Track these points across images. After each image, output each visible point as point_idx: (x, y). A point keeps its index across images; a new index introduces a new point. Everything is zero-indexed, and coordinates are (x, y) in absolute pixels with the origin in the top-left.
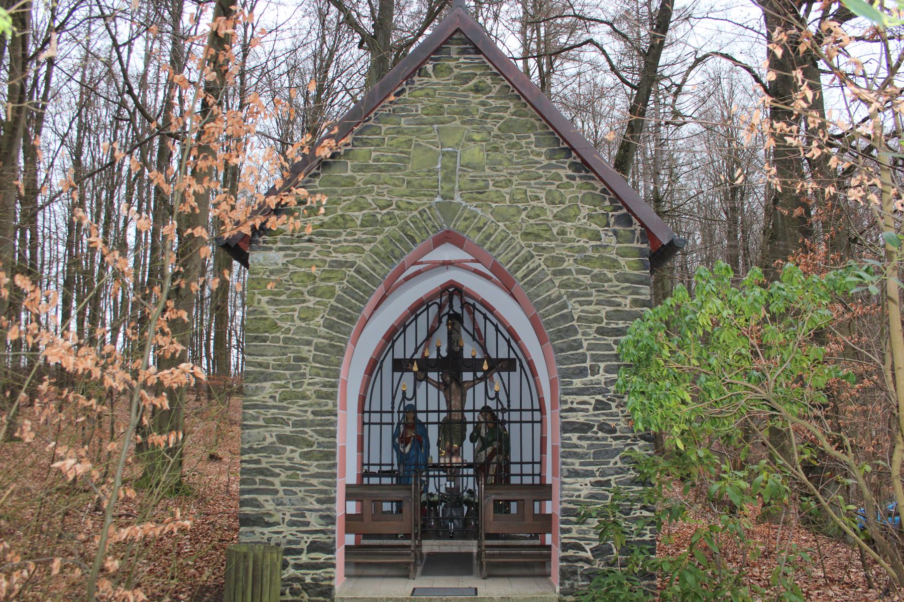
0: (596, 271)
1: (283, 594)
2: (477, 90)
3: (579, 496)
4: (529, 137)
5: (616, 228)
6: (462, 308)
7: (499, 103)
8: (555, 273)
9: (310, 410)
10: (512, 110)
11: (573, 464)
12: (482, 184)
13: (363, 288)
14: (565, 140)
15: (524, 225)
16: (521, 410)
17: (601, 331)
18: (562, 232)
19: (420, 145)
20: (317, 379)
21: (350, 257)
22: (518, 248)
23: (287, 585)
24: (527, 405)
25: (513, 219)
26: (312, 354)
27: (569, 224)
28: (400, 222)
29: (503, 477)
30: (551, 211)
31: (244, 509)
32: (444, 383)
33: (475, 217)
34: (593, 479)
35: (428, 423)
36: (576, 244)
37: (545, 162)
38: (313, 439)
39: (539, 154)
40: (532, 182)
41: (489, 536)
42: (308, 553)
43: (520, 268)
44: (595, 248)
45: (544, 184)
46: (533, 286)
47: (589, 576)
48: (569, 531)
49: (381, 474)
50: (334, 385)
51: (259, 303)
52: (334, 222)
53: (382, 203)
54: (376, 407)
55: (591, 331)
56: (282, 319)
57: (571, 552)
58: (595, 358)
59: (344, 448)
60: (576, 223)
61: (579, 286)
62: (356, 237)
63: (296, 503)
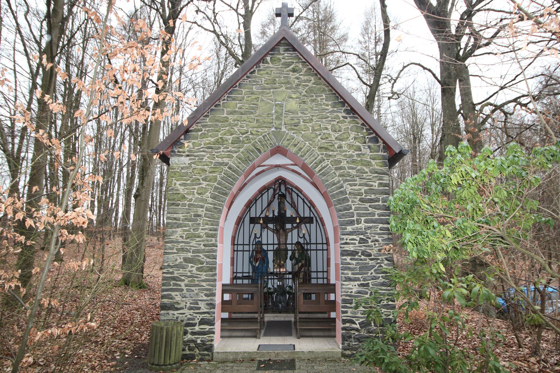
0: (359, 167)
1: (184, 350)
2: (294, 71)
3: (352, 292)
4: (322, 96)
5: (370, 144)
6: (286, 190)
7: (306, 78)
8: (336, 169)
9: (202, 243)
10: (313, 81)
11: (348, 274)
12: (297, 121)
13: (232, 177)
14: (342, 97)
15: (319, 143)
16: (317, 244)
17: (362, 200)
18: (340, 147)
19: (263, 100)
20: (207, 227)
21: (226, 160)
22: (316, 155)
23: (187, 345)
24: (319, 241)
25: (313, 140)
26: (204, 213)
27: (344, 142)
28: (253, 142)
29: (307, 279)
30: (334, 135)
31: (163, 300)
32: (276, 229)
33: (293, 139)
34: (359, 283)
35: (268, 250)
36: (348, 153)
37: (331, 109)
38: (204, 260)
39: (327, 105)
40: (324, 120)
41: (300, 313)
42: (199, 325)
43: (317, 166)
44: (358, 155)
45: (330, 121)
46: (324, 175)
47: (359, 339)
48: (346, 312)
49: (243, 278)
50: (216, 230)
51: (175, 185)
52: (217, 141)
53: (243, 131)
54: (241, 242)
55: (357, 200)
56: (188, 194)
57: (347, 325)
58: (359, 215)
59: (221, 265)
60: (348, 142)
61: (349, 176)
62: (229, 150)
63: (193, 296)
